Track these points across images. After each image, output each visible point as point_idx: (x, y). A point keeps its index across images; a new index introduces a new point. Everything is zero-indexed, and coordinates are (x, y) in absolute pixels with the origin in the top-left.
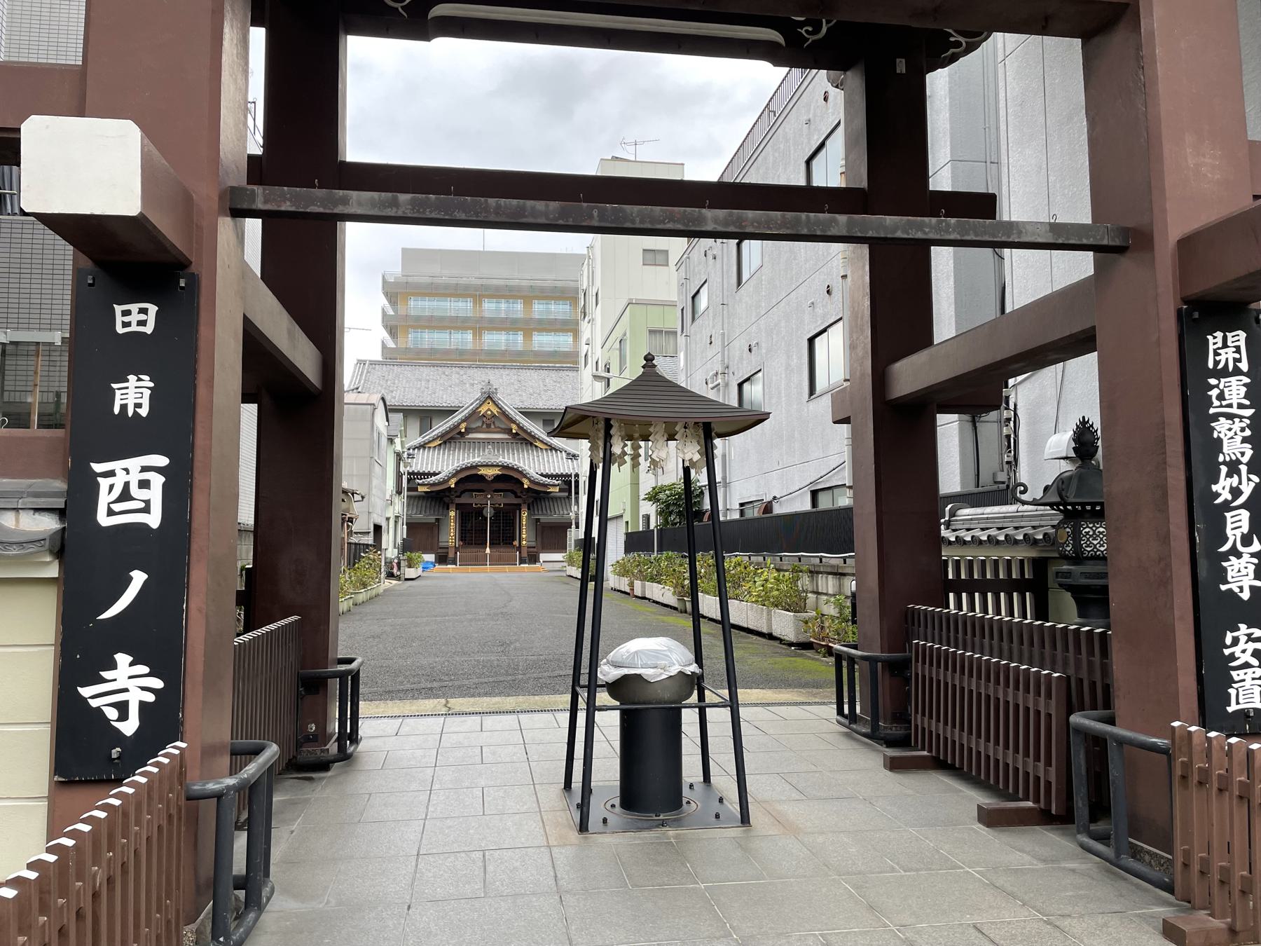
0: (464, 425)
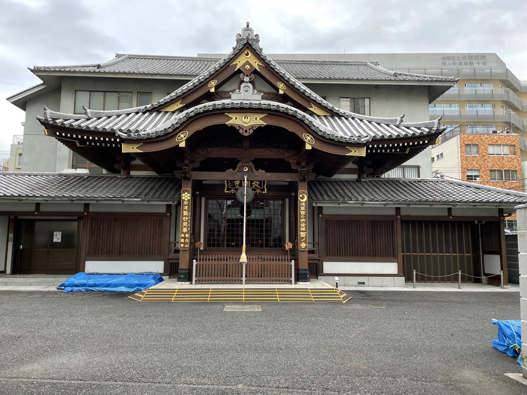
0: (213, 83)
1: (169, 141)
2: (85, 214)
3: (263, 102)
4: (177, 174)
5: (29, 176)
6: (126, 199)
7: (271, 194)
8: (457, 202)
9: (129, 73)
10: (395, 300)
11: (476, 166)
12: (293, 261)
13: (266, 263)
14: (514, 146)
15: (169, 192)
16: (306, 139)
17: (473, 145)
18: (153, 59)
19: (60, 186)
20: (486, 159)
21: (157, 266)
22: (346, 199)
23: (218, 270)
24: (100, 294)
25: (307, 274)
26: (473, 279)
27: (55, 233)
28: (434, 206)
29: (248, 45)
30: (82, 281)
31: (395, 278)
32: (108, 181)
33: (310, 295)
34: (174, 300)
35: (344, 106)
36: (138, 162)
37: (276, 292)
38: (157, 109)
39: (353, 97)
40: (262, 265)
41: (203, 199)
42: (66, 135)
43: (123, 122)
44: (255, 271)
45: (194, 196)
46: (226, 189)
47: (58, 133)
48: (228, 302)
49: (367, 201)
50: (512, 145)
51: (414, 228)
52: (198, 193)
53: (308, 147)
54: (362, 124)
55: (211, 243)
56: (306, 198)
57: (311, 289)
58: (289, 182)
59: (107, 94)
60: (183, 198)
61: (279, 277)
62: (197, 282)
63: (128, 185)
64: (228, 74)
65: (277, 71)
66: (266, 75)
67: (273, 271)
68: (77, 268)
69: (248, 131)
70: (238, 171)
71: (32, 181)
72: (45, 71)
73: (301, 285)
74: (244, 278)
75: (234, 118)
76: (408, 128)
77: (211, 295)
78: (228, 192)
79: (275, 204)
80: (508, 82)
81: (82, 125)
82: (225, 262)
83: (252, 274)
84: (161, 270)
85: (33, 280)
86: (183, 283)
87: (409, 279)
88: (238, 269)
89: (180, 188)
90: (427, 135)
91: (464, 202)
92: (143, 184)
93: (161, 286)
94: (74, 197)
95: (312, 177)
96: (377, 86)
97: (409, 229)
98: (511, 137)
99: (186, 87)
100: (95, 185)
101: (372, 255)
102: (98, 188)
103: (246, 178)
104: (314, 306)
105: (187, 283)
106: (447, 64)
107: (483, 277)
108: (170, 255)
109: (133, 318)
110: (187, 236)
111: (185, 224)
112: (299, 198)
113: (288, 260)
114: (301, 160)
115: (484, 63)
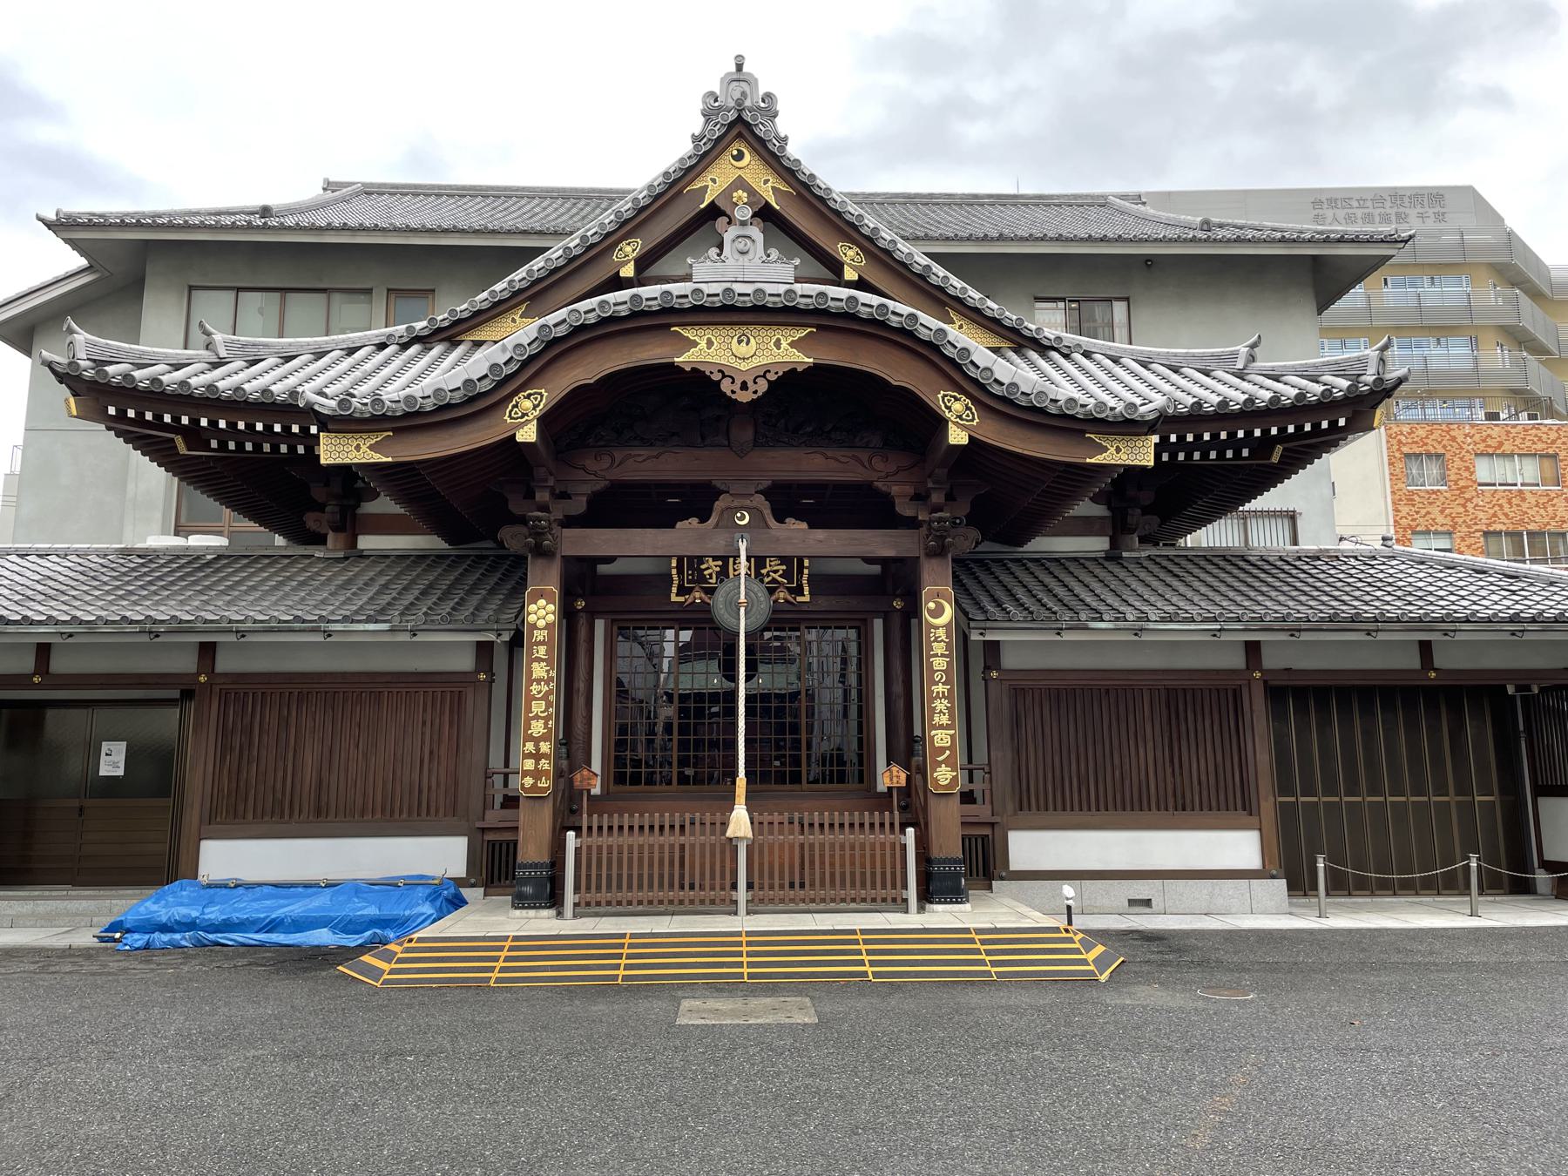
1: (483, 422)
2: (203, 679)
3: (800, 288)
4: (513, 539)
5: (21, 556)
6: (339, 627)
7: (824, 603)
8: (1458, 620)
9: (362, 229)
10: (1274, 968)
11: (1440, 519)
12: (910, 831)
13: (816, 837)
14: (1555, 456)
15: (485, 600)
16: (949, 408)
17: (1429, 455)
18: (439, 196)
19: (118, 588)
20: (1470, 500)
21: (445, 855)
22: (1083, 616)
23: (651, 865)
24: (243, 956)
25: (958, 875)
26: (1506, 881)
27: (105, 746)
28: (1381, 636)
29: (740, 126)
30: (184, 911)
31: (1254, 882)
32: (283, 569)
33: (978, 952)
34: (498, 980)
35: (1049, 321)
36: (384, 505)
37: (856, 942)
38: (449, 335)
39: (1076, 295)
40: (802, 846)
41: (600, 625)
42: (140, 414)
43: (332, 373)
44: (782, 866)
45: (568, 614)
46: (674, 590)
47: (112, 411)
48: (690, 986)
49: (1148, 624)
50: (1548, 456)
51: (1302, 711)
52: (581, 604)
53: (957, 437)
54: (1117, 370)
55: (628, 772)
56: (949, 612)
57: (979, 931)
58: (884, 561)
59: (291, 296)
60: (532, 618)
61: (863, 885)
62: (582, 909)
63: (349, 582)
64: (677, 217)
65: (837, 207)
66: (805, 219)
67: (843, 865)
68: (168, 865)
69: (750, 384)
70: (717, 526)
71: (29, 573)
72: (90, 225)
73: (942, 916)
74: (742, 894)
75: (703, 344)
76: (1276, 379)
77: (629, 957)
78: (681, 599)
79: (823, 648)
80: (1513, 270)
81: (194, 381)
82: (677, 839)
83: (771, 876)
84: (459, 869)
85: (27, 907)
86: (532, 913)
87: (1300, 885)
88: (723, 861)
89: (522, 584)
90: (1346, 398)
91: (1482, 620)
92: (397, 577)
93: (456, 925)
94: (162, 622)
95: (966, 541)
96: (1149, 262)
97: (1286, 713)
98: (1544, 429)
99: (542, 264)
100: (238, 583)
101: (1171, 805)
102: (246, 592)
103: (743, 547)
104: (1002, 998)
105: (545, 913)
106: (1329, 220)
107: (1542, 877)
108: (489, 814)
109: (337, 1065)
110: (545, 747)
111: (538, 707)
112: (926, 614)
113: (892, 825)
114: (930, 485)
115: (1440, 217)
